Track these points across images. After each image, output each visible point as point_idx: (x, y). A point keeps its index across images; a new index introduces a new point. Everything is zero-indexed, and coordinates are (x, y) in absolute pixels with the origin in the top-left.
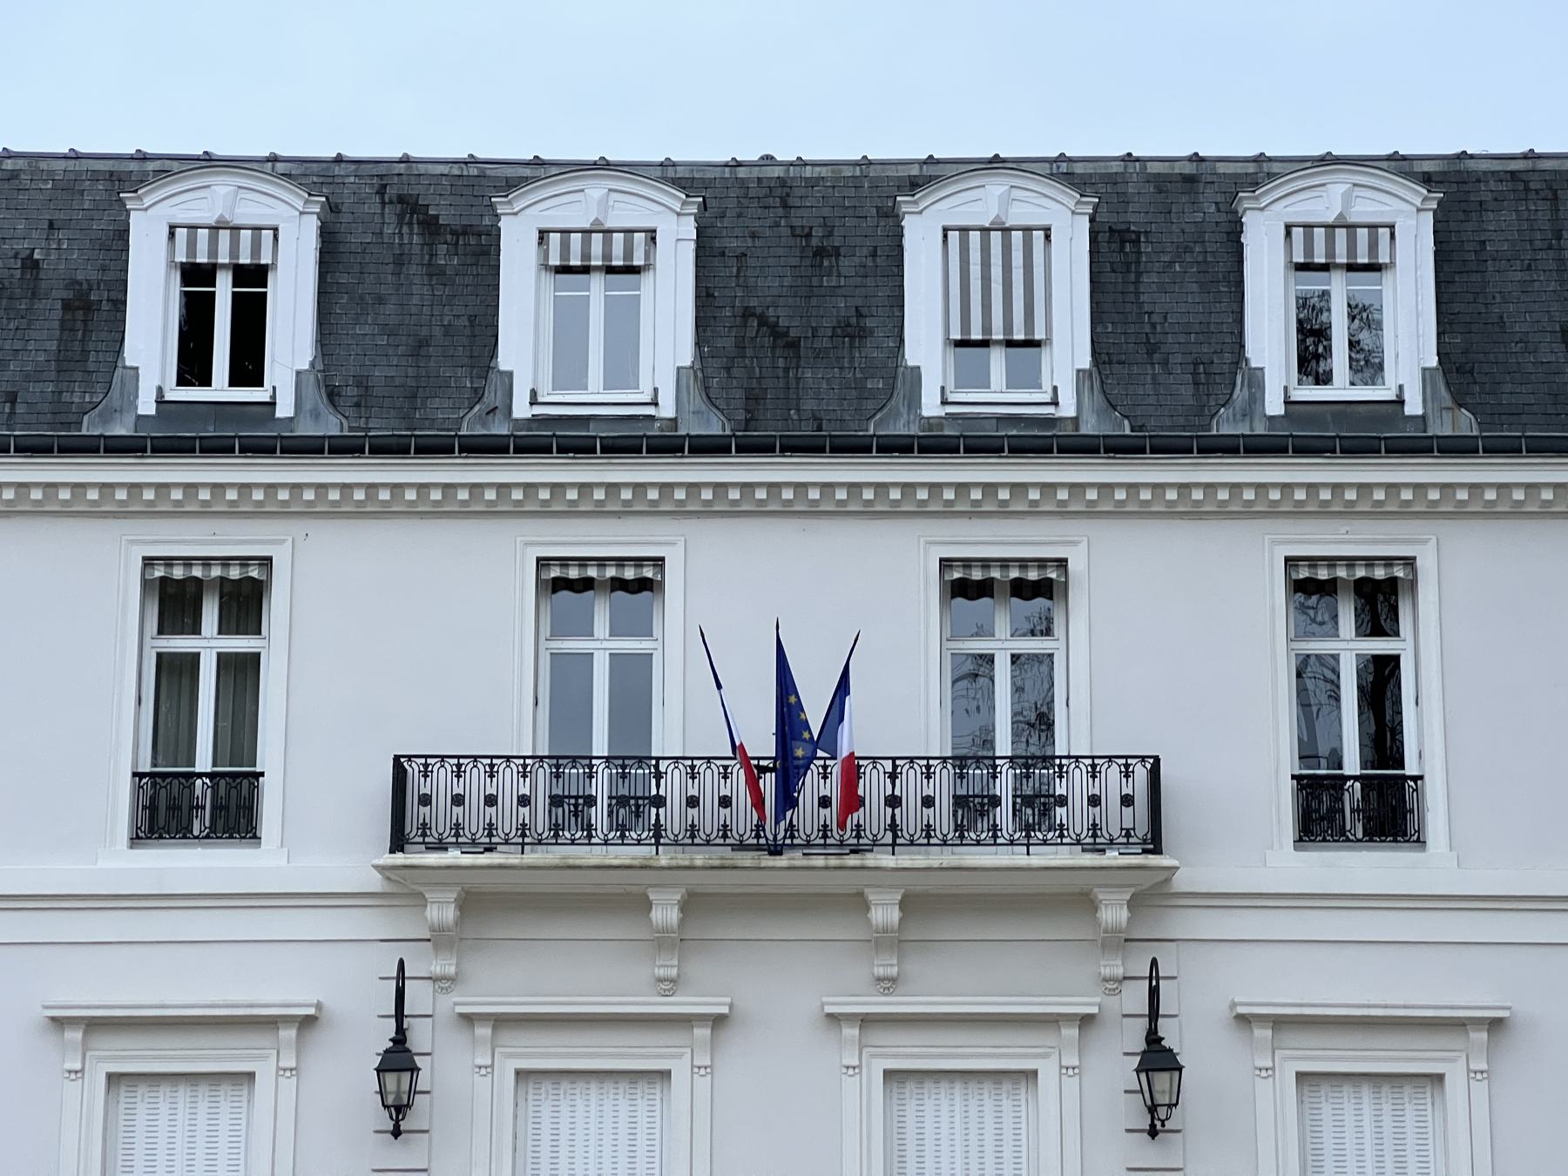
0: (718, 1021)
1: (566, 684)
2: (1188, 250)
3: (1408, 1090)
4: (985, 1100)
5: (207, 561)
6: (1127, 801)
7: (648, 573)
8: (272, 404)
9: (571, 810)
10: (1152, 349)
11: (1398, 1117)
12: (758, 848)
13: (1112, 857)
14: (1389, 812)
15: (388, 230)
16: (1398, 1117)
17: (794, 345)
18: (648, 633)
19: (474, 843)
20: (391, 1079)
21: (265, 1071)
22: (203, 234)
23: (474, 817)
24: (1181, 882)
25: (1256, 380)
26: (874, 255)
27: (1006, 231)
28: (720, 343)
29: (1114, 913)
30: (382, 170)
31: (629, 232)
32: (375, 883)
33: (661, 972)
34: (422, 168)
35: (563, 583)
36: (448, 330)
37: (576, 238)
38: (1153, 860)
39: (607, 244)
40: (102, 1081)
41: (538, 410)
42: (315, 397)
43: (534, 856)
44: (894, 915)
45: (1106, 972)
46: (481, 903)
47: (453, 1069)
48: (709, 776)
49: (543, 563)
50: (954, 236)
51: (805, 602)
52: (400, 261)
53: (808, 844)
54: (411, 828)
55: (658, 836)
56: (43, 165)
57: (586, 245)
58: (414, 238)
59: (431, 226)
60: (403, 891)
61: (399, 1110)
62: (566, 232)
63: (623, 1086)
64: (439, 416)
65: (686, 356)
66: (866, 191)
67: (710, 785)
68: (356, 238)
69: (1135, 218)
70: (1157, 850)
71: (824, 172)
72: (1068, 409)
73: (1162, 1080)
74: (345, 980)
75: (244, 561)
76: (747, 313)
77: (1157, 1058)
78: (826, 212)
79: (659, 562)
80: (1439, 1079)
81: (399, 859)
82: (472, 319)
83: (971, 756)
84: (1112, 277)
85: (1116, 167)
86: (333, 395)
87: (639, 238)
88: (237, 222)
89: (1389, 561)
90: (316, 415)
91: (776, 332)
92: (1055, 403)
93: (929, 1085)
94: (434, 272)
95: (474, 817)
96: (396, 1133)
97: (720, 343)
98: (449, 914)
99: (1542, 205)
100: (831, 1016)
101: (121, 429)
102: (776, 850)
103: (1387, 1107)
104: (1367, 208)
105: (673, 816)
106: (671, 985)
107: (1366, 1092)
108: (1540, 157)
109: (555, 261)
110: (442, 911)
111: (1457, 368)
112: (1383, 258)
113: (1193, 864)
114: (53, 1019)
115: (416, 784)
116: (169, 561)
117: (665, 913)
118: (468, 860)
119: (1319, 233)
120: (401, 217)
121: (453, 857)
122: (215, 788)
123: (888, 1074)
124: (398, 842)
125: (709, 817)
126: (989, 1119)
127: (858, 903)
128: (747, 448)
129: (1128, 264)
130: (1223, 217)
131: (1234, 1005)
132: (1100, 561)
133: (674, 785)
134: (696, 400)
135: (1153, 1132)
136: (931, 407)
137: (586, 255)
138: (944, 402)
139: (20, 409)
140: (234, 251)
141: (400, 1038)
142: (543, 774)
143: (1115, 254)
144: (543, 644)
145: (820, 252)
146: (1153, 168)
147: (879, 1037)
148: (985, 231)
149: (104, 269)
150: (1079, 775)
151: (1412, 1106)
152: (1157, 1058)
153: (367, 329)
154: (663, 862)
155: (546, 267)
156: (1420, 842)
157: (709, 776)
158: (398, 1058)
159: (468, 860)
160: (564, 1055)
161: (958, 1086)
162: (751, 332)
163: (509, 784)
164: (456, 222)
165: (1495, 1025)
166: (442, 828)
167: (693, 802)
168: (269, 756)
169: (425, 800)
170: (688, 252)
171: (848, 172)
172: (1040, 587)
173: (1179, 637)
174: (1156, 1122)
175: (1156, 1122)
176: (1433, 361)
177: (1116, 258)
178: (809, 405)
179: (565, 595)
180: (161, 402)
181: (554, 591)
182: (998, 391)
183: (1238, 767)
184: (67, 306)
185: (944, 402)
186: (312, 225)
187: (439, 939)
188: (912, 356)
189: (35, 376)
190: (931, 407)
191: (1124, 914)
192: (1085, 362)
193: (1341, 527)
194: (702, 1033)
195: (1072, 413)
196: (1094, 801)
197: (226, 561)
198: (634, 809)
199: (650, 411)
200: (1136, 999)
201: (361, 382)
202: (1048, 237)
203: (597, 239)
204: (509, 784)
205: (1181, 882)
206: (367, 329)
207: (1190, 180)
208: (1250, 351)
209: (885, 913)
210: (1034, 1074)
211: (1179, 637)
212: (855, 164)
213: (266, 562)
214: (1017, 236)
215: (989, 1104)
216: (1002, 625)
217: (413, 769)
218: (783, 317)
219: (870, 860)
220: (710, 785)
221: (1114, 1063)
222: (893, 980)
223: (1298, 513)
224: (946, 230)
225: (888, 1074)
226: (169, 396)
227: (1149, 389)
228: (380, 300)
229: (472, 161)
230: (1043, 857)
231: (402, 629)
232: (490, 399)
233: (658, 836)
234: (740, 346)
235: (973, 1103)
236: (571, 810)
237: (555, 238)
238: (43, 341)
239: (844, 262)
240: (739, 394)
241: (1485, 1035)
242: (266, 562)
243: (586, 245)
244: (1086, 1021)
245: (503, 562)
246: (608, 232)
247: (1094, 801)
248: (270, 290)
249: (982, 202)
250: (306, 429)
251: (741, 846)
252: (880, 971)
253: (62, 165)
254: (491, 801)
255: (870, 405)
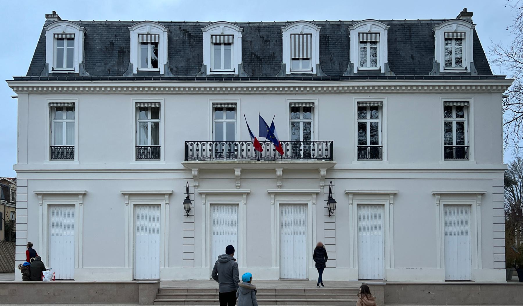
0: (248, 194)
1: (218, 128)
2: (338, 40)
3: (377, 207)
4: (298, 209)
5: (148, 103)
6: (326, 150)
7: (234, 106)
8: (159, 71)
9: (219, 154)
10: (331, 60)
11: (375, 211)
12: (255, 159)
13: (323, 161)
14: (375, 153)
15: (181, 36)
16: (375, 211)
17: (261, 60)
18: (234, 119)
19: (201, 159)
20: (186, 205)
21: (163, 204)
22: (145, 36)
23: (201, 153)
24: (336, 167)
25: (352, 66)
26: (276, 41)
27: (303, 35)
28: (246, 60)
29: (323, 173)
30: (180, 24)
31: (229, 35)
32: (182, 167)
33: (237, 185)
34: (188, 24)
35: (217, 108)
36: (194, 57)
37: (218, 37)
38: (331, 161)
39: (224, 38)
40: (132, 206)
41: (212, 73)
42: (168, 70)
43: (212, 161)
44: (281, 173)
45: (321, 184)
46: (202, 171)
47: (197, 202)
48: (246, 145)
49: (213, 104)
50: (293, 36)
51: (264, 107)
52: (184, 43)
53: (265, 159)
54: (189, 157)
55: (236, 157)
56: (114, 24)
57: (220, 38)
58: (186, 39)
59: (190, 36)
60: (188, 169)
61: (188, 211)
62: (216, 36)
63: (230, 207)
64: (192, 74)
65: (240, 62)
66: (275, 29)
67: (246, 147)
68: (175, 38)
69: (328, 33)
70: (332, 160)
71: (267, 24)
72: (315, 72)
73: (332, 205)
74: (176, 185)
75: (155, 103)
76: (252, 54)
77: (331, 200)
78: (267, 33)
79: (236, 104)
80: (383, 205)
81: (186, 162)
82: (198, 55)
83: (295, 143)
84: (323, 46)
85: (324, 23)
86: (171, 70)
87: (231, 37)
88: (151, 33)
89: (377, 102)
90: (168, 74)
91: (258, 58)
92: (312, 71)
93: (287, 207)
94: (191, 45)
95: (201, 153)
96: (188, 215)
97: (246, 60)
98: (197, 173)
99: (408, 31)
100: (269, 193)
101: (131, 76)
102: (259, 160)
103: (373, 211)
104: (375, 30)
105: (239, 153)
106: (239, 187)
107: (369, 208)
108: (407, 21)
109: (214, 42)
110: (195, 172)
111: (391, 64)
112: (378, 40)
113: (339, 163)
114: (123, 194)
115: (190, 147)
116: (140, 103)
117: (238, 173)
118: (200, 162)
119: (365, 35)
120: (184, 34)
121: (197, 161)
122: (151, 149)
123: (280, 204)
124: (186, 159)
125: (246, 153)
126: (298, 213)
127: (274, 171)
128: (252, 79)
129: (326, 43)
130: (345, 33)
131: (346, 191)
132: (321, 103)
133: (239, 147)
134: (242, 71)
135: (330, 215)
136: (288, 72)
137: (220, 40)
138: (291, 71)
139: (111, 73)
140: (151, 40)
141: (188, 197)
142: (214, 145)
143: (324, 40)
144: (214, 121)
145: (266, 41)
146: (331, 23)
147: (279, 197)
148: (299, 35)
149: (126, 44)
150: (317, 145)
151: (378, 210)
152: (331, 200)
153: (178, 57)
154: (237, 162)
155: (213, 43)
156: (381, 159)
157: (246, 145)
158: (187, 201)
159: (200, 162)
160: (220, 201)
161: (293, 207)
162: (253, 57)
163: (207, 147)
164: (194, 35)
165: (395, 194)
166: (195, 156)
167: (243, 150)
168: (161, 143)
169: (191, 150)
170: (240, 40)
171: (271, 24)
172: (309, 109)
173: (335, 118)
174: (330, 213)
175: (330, 213)
176: (387, 62)
177: (324, 42)
178: (264, 72)
179: (218, 112)
180: (138, 71)
181: (216, 111)
182: (301, 67)
183: (347, 144)
184: (119, 52)
185: (291, 71)
186: (166, 34)
187: (195, 178)
188: (284, 61)
189: (113, 66)
190: (288, 72)
191: (325, 173)
192: (318, 63)
193: (369, 96)
194: (167, 197)
195: (315, 73)
196: (320, 150)
197: (151, 103)
198: (231, 155)
199: (233, 73)
200: (327, 190)
201: (177, 67)
202: (311, 36)
203: (222, 37)
204: (207, 147)
205: (336, 167)
206: (178, 57)
207: (339, 25)
208: (351, 60)
209: (279, 173)
210: (307, 204)
211: (335, 118)
212: (273, 23)
213: (159, 104)
214: (305, 36)
215: (298, 210)
216: (301, 117)
217: (188, 144)
218: (259, 54)
219: (277, 162)
220: (246, 147)
221: (323, 203)
222: (281, 186)
223: (360, 93)
224: (291, 35)
225: (280, 204)
226: (139, 70)
227: (331, 68)
228: (180, 51)
229: (197, 22)
230: (309, 161)
231: (187, 117)
232: (202, 71)
233: (236, 157)
234: (251, 60)
235: (295, 210)
236: (219, 154)
237: (214, 37)
238: (115, 59)
239: (271, 43)
240: (251, 70)
241: (246, 196)
242: (159, 104)
243: (220, 38)
244: (317, 194)
245: (206, 103)
246: (224, 35)
247: (320, 150)
248: (158, 48)
249: (298, 29)
250: (166, 76)
251: (252, 159)
252: (278, 184)
253: (117, 24)
254: (204, 150)
255: (276, 72)
